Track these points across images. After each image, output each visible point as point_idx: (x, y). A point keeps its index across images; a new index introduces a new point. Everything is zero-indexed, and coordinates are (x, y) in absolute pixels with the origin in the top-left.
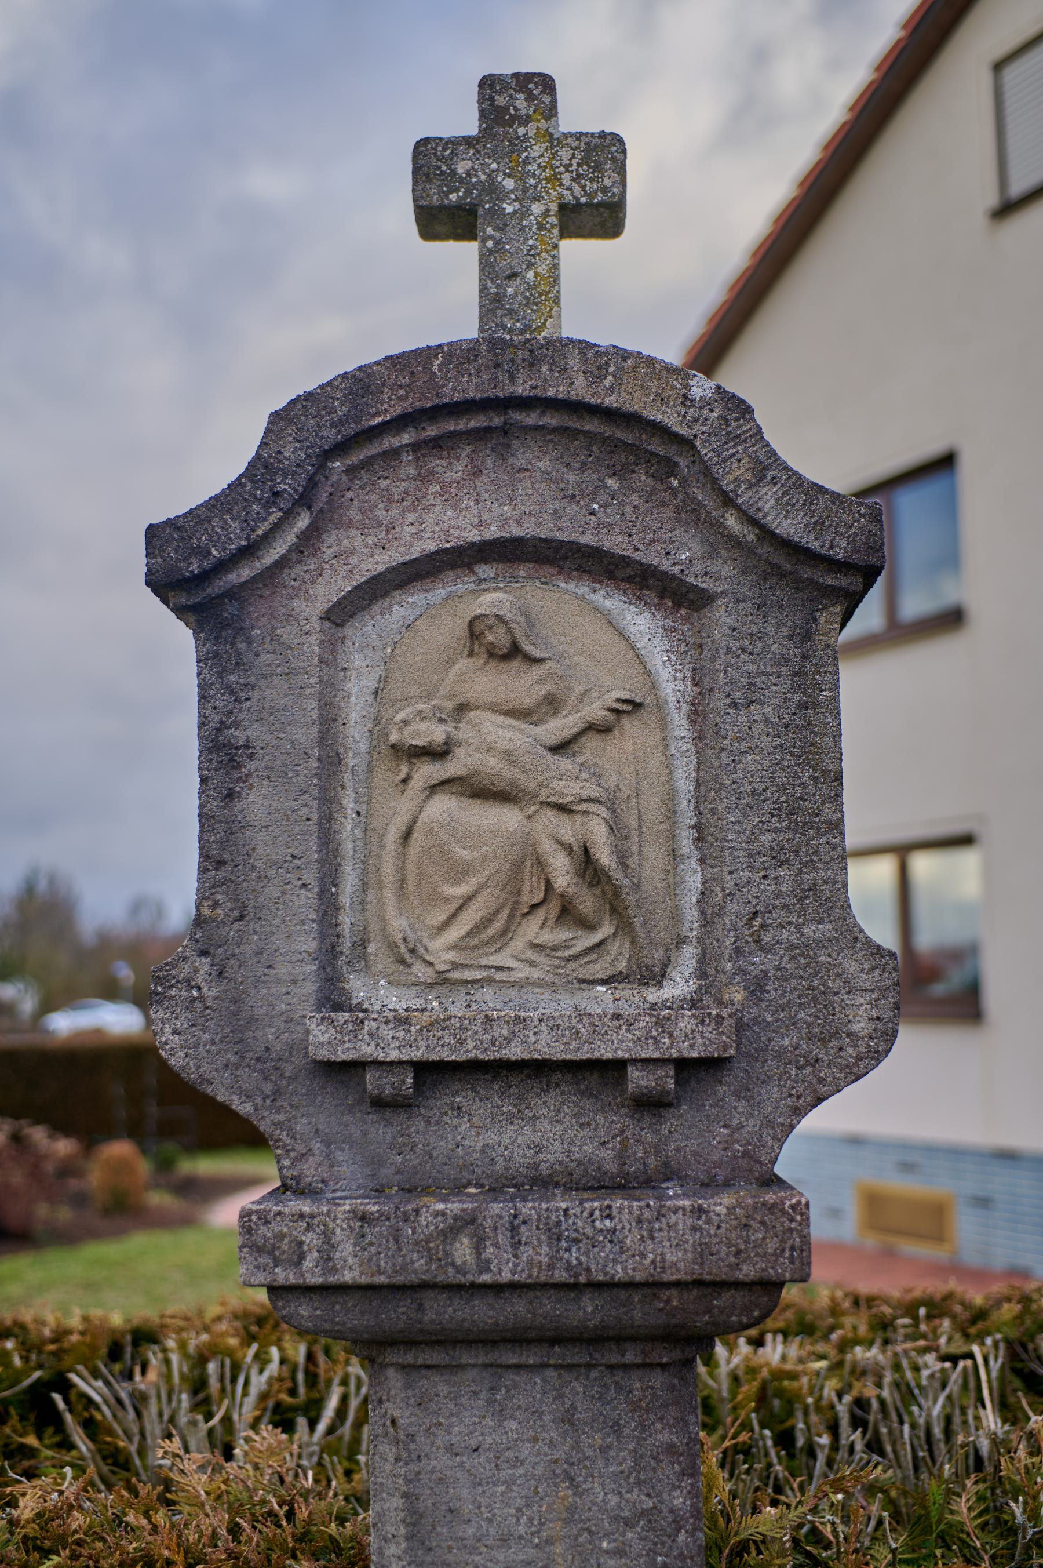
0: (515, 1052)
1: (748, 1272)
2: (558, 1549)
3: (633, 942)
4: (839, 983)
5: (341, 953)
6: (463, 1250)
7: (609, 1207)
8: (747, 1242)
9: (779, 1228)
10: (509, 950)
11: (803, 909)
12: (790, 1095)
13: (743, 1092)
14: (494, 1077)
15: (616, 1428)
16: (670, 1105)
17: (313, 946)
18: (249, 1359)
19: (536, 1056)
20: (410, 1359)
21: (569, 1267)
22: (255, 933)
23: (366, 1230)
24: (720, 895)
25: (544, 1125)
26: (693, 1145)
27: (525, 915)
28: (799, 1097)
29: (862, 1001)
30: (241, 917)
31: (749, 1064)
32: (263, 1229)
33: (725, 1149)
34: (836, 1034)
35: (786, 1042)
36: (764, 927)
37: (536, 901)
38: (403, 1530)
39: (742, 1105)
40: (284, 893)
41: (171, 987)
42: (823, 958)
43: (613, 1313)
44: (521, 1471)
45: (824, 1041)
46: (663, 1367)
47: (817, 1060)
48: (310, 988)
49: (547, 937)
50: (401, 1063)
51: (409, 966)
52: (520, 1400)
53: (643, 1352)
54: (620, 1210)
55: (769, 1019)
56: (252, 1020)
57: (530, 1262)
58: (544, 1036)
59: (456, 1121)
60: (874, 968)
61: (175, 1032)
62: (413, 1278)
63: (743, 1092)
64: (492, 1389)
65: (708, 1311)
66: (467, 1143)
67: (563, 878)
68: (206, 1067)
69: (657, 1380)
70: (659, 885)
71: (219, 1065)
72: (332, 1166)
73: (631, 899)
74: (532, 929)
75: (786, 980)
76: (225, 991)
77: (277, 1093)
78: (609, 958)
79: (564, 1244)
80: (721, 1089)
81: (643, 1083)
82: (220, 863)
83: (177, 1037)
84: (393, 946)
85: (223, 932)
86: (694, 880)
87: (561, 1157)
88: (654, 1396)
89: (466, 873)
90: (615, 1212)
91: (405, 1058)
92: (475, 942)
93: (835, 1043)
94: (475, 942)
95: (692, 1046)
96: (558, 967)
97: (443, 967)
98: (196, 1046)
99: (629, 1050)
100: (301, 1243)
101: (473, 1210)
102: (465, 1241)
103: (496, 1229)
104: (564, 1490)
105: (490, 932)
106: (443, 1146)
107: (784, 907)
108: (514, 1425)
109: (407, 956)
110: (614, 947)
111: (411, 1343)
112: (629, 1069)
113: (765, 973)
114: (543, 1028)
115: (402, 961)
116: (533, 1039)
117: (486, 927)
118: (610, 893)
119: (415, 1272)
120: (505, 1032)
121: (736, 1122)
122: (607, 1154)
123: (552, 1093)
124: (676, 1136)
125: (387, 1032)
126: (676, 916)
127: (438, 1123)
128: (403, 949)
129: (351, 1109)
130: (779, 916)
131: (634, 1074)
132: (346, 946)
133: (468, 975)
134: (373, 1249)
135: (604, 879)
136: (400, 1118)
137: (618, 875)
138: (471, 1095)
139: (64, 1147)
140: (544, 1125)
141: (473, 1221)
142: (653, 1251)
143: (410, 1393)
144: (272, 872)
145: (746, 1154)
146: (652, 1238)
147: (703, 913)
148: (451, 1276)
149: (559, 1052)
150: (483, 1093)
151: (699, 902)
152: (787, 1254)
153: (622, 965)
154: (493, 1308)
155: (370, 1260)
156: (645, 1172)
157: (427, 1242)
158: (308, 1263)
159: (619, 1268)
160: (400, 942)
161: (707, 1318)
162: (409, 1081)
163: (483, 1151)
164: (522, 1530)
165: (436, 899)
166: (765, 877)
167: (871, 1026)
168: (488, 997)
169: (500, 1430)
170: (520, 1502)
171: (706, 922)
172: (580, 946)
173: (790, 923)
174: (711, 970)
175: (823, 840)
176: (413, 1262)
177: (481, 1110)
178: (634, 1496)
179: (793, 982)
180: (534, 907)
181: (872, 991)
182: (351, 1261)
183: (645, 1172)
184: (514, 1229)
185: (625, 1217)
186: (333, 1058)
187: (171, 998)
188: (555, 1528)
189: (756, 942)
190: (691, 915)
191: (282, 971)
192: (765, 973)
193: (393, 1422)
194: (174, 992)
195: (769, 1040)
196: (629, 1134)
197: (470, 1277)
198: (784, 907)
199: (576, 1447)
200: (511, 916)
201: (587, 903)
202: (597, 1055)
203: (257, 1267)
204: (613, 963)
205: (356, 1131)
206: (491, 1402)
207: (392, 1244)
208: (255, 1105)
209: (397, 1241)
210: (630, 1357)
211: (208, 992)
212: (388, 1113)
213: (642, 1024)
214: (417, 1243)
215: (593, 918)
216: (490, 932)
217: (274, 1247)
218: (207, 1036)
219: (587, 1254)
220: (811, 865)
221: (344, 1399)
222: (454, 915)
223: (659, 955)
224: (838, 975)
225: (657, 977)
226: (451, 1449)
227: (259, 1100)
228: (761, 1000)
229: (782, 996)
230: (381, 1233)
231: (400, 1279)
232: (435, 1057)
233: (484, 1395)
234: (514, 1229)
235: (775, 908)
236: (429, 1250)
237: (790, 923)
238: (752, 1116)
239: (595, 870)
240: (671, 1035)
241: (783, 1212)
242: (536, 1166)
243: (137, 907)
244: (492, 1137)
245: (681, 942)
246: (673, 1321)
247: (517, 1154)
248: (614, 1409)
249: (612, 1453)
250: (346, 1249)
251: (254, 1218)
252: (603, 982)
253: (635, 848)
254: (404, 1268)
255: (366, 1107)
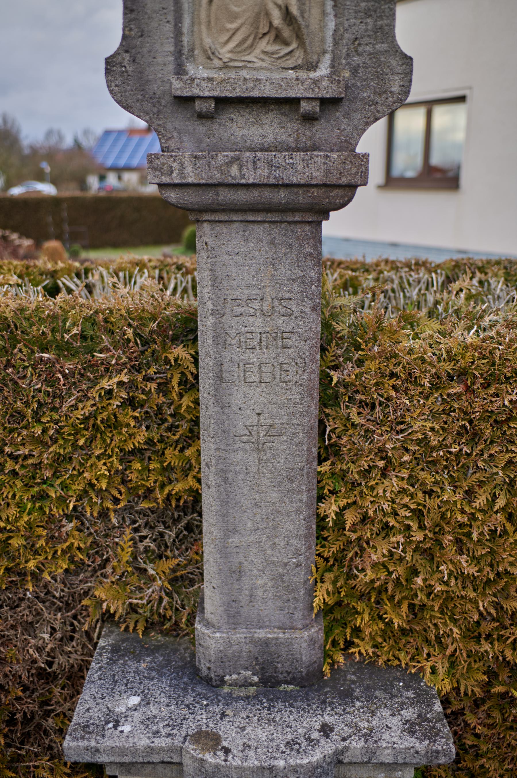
0: (256, 93)
1: (344, 181)
2: (268, 290)
3: (305, 52)
4: (388, 70)
5: (183, 54)
6: (234, 170)
7: (292, 154)
8: (344, 169)
9: (357, 164)
10: (253, 54)
11: (376, 37)
12: (365, 117)
13: (347, 116)
14: (247, 107)
15: (291, 246)
16: (316, 119)
17: (172, 49)
18: (136, 272)
19: (265, 95)
20: (213, 218)
21: (275, 178)
22: (148, 43)
23: (197, 162)
24: (342, 30)
25: (266, 127)
26: (325, 136)
27: (261, 38)
28: (368, 118)
29: (397, 78)
30: (142, 36)
31: (349, 103)
32: (157, 161)
33: (338, 139)
34: (385, 92)
35: (365, 95)
36: (359, 44)
37: (265, 31)
38: (210, 283)
39: (345, 121)
40: (159, 25)
41: (114, 66)
42: (383, 59)
43: (292, 197)
44: (254, 261)
45: (380, 95)
46: (309, 222)
47: (377, 103)
48: (171, 67)
49: (270, 48)
50: (209, 98)
51: (212, 60)
52: (254, 235)
53: (302, 216)
54: (296, 156)
55: (359, 85)
56: (148, 81)
57: (260, 175)
58: (268, 87)
59: (231, 125)
60: (403, 64)
61: (116, 86)
62: (215, 181)
63: (347, 116)
64: (244, 231)
65: (328, 197)
66: (235, 134)
67: (277, 20)
68: (129, 101)
69: (307, 228)
70: (317, 27)
71: (135, 100)
72: (181, 143)
73: (305, 31)
74: (263, 45)
75: (367, 68)
76: (136, 68)
77: (159, 112)
78: (295, 58)
79: (274, 168)
80: (338, 114)
81: (307, 108)
82: (132, 11)
83: (117, 88)
84: (205, 51)
85: (134, 42)
86: (331, 25)
87: (273, 140)
88: (306, 235)
89: (236, 18)
90: (294, 156)
91: (211, 95)
92: (239, 49)
93: (385, 96)
94: (239, 49)
95: (327, 92)
96: (273, 62)
97: (226, 60)
98: (125, 92)
99: (302, 94)
100: (172, 167)
101: (239, 155)
102: (236, 167)
103: (247, 162)
104: (270, 269)
105: (246, 45)
106: (226, 135)
107: (369, 36)
108: (252, 245)
109: (211, 56)
110: (297, 53)
111: (214, 211)
112: (302, 102)
113: (359, 65)
114: (268, 83)
115: (209, 58)
116: (263, 88)
117: (244, 43)
118: (296, 28)
119: (216, 179)
120: (252, 85)
121: (343, 127)
122: (291, 139)
123: (270, 114)
124: (319, 133)
125: (204, 84)
126: (323, 41)
127: (224, 125)
128: (209, 52)
129: (189, 119)
130: (366, 40)
131: (303, 104)
132: (185, 51)
133: (236, 64)
134: (199, 170)
135: (294, 21)
136: (209, 123)
137: (300, 19)
138: (237, 114)
139: (27, 243)
140: (266, 127)
141: (238, 159)
142: (308, 172)
143: (213, 232)
144: (154, 15)
145: (346, 141)
146: (308, 167)
147: (334, 39)
148: (230, 180)
149: (274, 94)
150: (242, 113)
151: (333, 34)
152: (359, 174)
153: (300, 62)
154: (246, 195)
155: (198, 174)
156: (306, 147)
157: (221, 167)
158: (174, 175)
159: (295, 178)
160: (208, 49)
161: (327, 200)
162: (213, 105)
163: (242, 137)
164: (254, 283)
165: (223, 30)
166: (361, 22)
167: (400, 89)
168: (244, 73)
169: (246, 247)
170: (254, 273)
171: (336, 43)
172: (283, 52)
173: (370, 43)
174: (336, 64)
175: (387, 6)
176: (215, 175)
177: (241, 120)
178: (296, 271)
179: (370, 69)
180: (264, 34)
181: (401, 74)
182: (191, 174)
183: (306, 147)
184: (254, 162)
185: (298, 158)
186: (182, 95)
187: (114, 71)
188: (266, 282)
189: (356, 51)
190: (329, 41)
191: (160, 60)
192: (359, 65)
193: (206, 244)
194: (115, 68)
195: (358, 94)
196: (300, 131)
197: (237, 181)
198: (369, 36)
199: (275, 253)
200: (255, 39)
201: (286, 33)
202: (289, 95)
203: (155, 176)
204: (296, 61)
205: (191, 128)
206: (243, 236)
207: (207, 168)
208: (150, 117)
209: (209, 166)
210: (297, 218)
211: (130, 69)
212: (204, 121)
213: (307, 83)
214: (217, 167)
215: (289, 40)
216: (246, 45)
217: (161, 168)
218: (129, 88)
219: (282, 172)
220: (381, 17)
221: (176, 284)
222: (231, 38)
223: (315, 57)
224: (388, 67)
225: (313, 67)
226: (228, 253)
227: (151, 115)
228: (356, 76)
229: (365, 75)
230: (203, 163)
231: (210, 181)
232: (223, 95)
233: (241, 233)
234: (254, 162)
235: (365, 36)
236: (222, 170)
237: (370, 43)
238: (349, 125)
239: (291, 18)
240: (319, 88)
241: (359, 158)
242: (263, 144)
243: (49, 133)
244: (245, 131)
245: (324, 52)
246: (314, 201)
247: (255, 138)
248: (290, 239)
249: (289, 255)
250: (189, 169)
251: (153, 157)
252: (292, 69)
253: (307, 9)
254: (212, 177)
255: (195, 118)
